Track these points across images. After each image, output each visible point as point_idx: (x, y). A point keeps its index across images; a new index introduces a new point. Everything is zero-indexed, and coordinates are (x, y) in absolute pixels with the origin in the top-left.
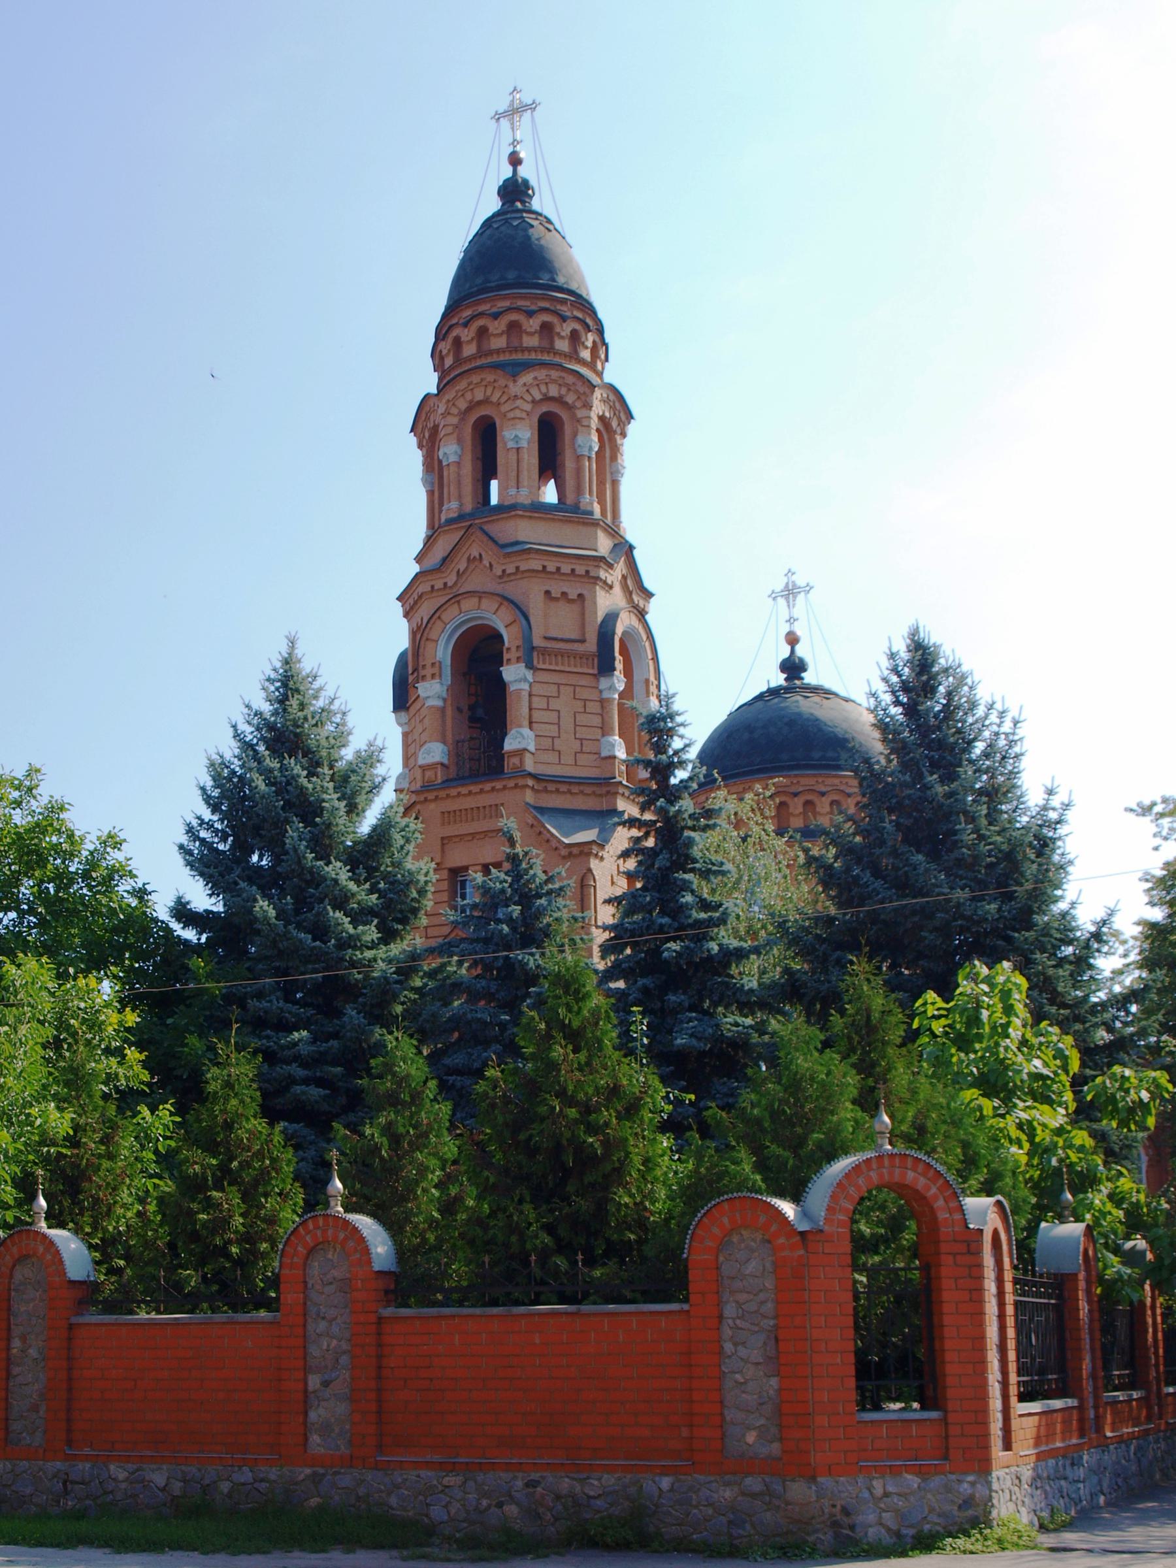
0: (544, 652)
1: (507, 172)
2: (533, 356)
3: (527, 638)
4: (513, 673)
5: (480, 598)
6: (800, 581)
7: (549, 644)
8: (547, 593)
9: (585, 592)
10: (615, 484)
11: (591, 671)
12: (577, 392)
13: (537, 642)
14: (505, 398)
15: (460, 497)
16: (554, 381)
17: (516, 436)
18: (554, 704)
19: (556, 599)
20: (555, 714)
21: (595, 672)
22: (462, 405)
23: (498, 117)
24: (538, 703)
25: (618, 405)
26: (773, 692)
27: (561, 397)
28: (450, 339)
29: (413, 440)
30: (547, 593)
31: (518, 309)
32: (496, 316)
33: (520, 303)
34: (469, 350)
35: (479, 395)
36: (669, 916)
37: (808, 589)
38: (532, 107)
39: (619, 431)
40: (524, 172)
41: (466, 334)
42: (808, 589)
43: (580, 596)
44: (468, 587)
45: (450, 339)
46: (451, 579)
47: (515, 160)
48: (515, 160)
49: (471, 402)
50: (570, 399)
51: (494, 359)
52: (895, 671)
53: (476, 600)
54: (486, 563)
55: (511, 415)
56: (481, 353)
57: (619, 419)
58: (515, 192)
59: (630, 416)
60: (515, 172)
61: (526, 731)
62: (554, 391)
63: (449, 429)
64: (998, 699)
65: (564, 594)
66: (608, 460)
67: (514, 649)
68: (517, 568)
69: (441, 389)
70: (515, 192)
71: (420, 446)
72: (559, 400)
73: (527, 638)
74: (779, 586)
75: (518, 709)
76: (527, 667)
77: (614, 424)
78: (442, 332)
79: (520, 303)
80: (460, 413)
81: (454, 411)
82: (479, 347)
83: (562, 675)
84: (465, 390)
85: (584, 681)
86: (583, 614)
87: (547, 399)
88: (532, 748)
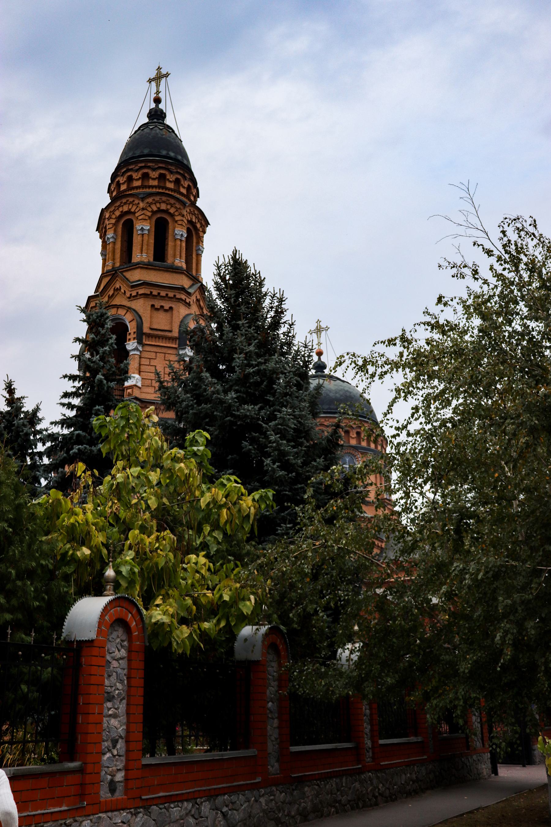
0: (149, 336)
1: (153, 105)
2: (154, 190)
3: (140, 327)
4: (131, 345)
5: (118, 308)
6: (323, 325)
7: (151, 332)
8: (153, 306)
9: (173, 306)
10: (199, 256)
11: (174, 346)
12: (176, 207)
13: (146, 330)
14: (138, 209)
15: (114, 259)
16: (164, 202)
17: (142, 228)
18: (153, 363)
19: (157, 309)
20: (154, 368)
21: (176, 346)
22: (118, 213)
23: (150, 81)
24: (144, 361)
25: (200, 217)
26: (145, 125)
27: (168, 210)
28: (115, 183)
29: (98, 234)
30: (153, 306)
31: (149, 167)
32: (154, 170)
33: (149, 164)
34: (123, 187)
35: (125, 208)
36: (81, 420)
37: (327, 329)
38: (167, 75)
39: (201, 230)
40: (161, 106)
41: (122, 180)
42: (327, 329)
43: (171, 308)
44: (114, 303)
45: (115, 183)
46: (106, 299)
47: (157, 101)
48: (157, 101)
49: (122, 212)
50: (172, 211)
51: (151, 190)
52: (223, 278)
53: (115, 309)
54: (122, 291)
55: (140, 218)
56: (129, 188)
57: (201, 224)
58: (157, 115)
59: (207, 223)
60: (157, 106)
61: (137, 376)
62: (163, 207)
63: (111, 226)
64: (277, 291)
65: (162, 307)
66: (194, 244)
67: (132, 334)
68: (137, 293)
69: (114, 200)
70: (157, 115)
71: (101, 237)
72: (166, 212)
73: (140, 327)
74: (313, 327)
75: (133, 364)
76: (138, 343)
77: (198, 225)
78: (114, 176)
79: (149, 164)
80: (116, 218)
81: (114, 217)
82: (128, 186)
83: (158, 348)
84: (119, 206)
85: (170, 351)
86: (172, 317)
87: (160, 211)
88: (139, 384)
